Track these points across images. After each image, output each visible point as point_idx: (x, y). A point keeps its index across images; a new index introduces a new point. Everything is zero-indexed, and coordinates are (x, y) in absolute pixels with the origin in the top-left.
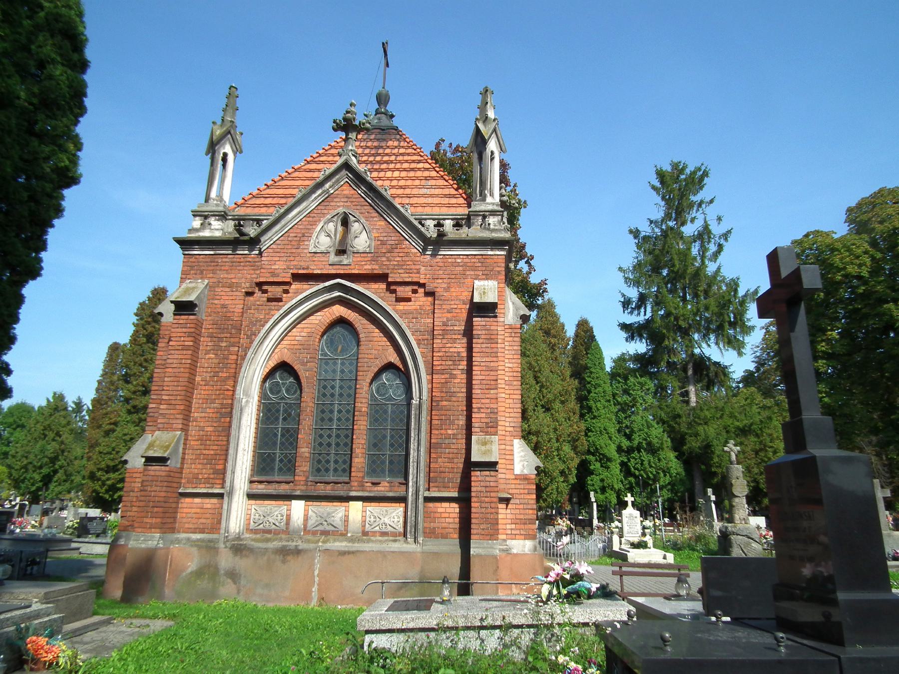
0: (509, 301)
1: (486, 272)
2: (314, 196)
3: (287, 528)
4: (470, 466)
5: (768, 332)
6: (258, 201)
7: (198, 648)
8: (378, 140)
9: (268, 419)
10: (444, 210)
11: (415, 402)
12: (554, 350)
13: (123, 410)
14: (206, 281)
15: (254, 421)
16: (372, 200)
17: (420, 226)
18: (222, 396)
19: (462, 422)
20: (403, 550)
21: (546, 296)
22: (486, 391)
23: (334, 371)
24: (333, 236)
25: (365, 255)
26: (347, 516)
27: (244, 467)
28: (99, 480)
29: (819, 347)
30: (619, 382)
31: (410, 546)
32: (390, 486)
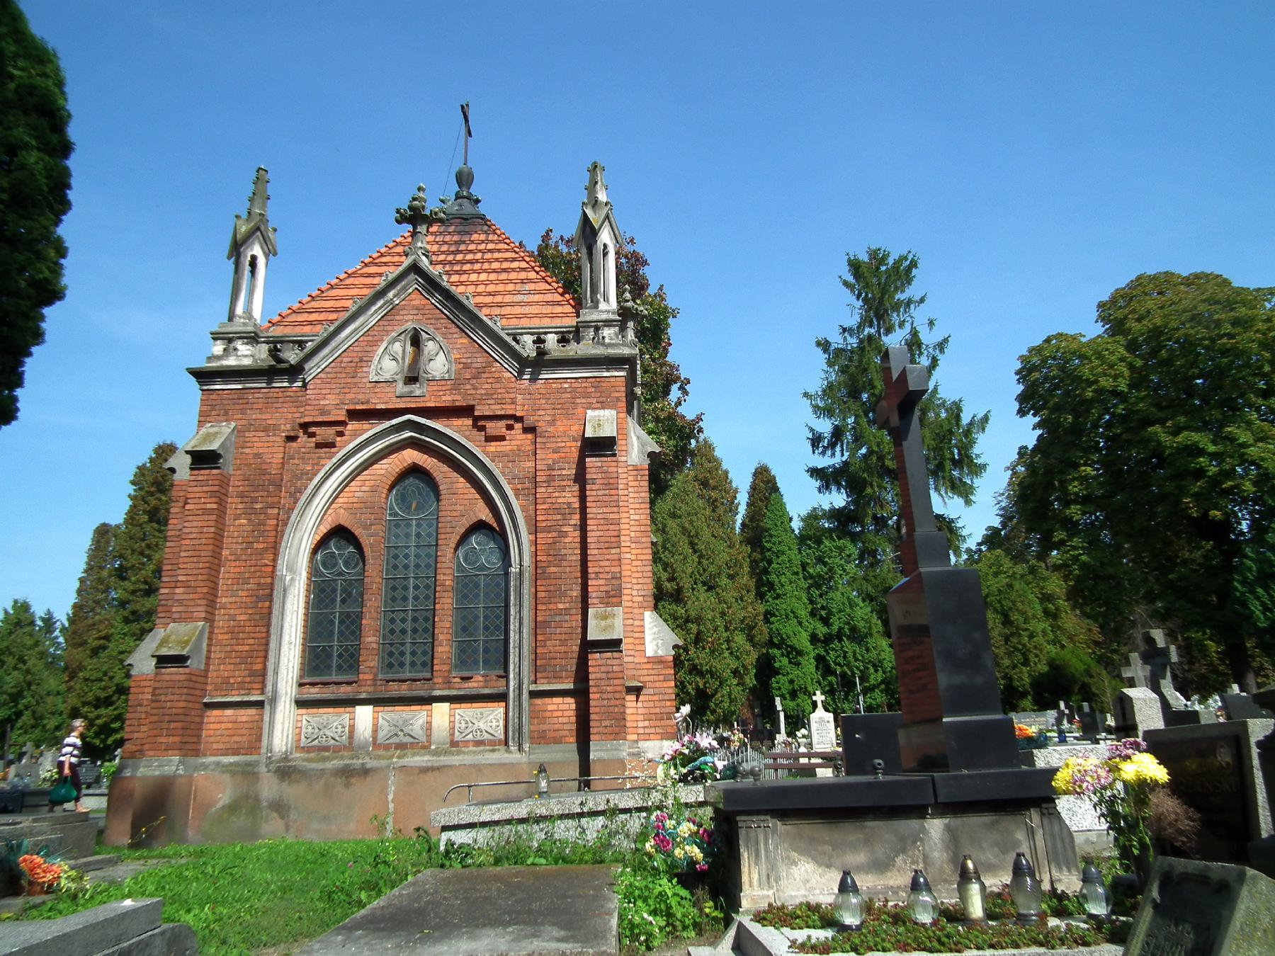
1: (601, 399)
2: (374, 308)
3: (350, 743)
4: (588, 647)
5: (1015, 473)
6: (300, 318)
8: (459, 233)
9: (321, 601)
13: (118, 618)
14: (233, 424)
15: (302, 605)
17: (514, 343)
18: (258, 574)
19: (576, 592)
20: (503, 761)
21: (702, 437)
25: (443, 383)
26: (429, 723)
27: (291, 666)
29: (1070, 487)
30: (810, 548)
31: (514, 756)
32: (486, 681)
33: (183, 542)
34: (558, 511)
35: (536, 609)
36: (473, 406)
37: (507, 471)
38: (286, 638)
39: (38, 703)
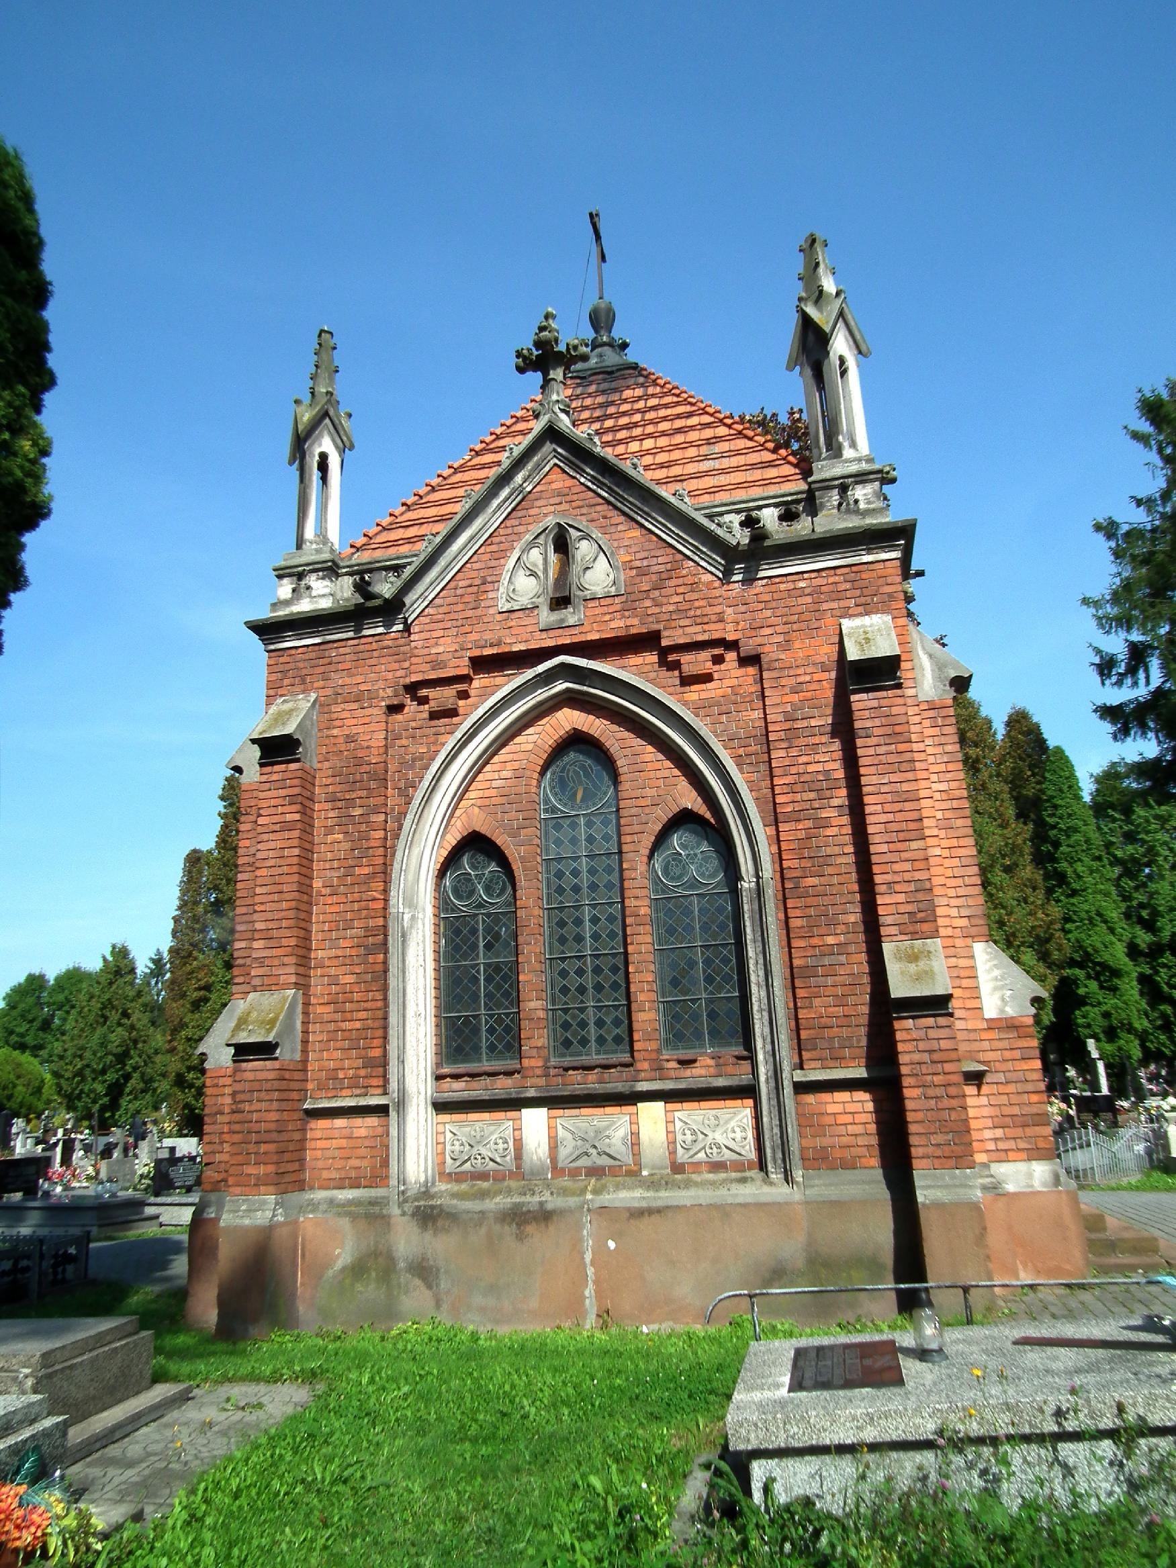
0: (921, 653)
1: (863, 600)
2: (495, 503)
3: (518, 1167)
6: (393, 535)
7: (358, 1474)
8: (603, 392)
9: (457, 948)
10: (756, 492)
11: (747, 884)
12: (978, 770)
14: (313, 696)
15: (430, 956)
16: (611, 491)
19: (854, 916)
20: (763, 1199)
22: (900, 846)
23: (574, 841)
24: (540, 574)
25: (609, 601)
26: (635, 1135)
27: (421, 1048)
28: (191, 1086)
30: (1114, 820)
31: (776, 1191)
33: (258, 873)
34: (809, 786)
35: (790, 947)
36: (659, 631)
37: (719, 728)
38: (411, 1010)
39: (146, 1064)
